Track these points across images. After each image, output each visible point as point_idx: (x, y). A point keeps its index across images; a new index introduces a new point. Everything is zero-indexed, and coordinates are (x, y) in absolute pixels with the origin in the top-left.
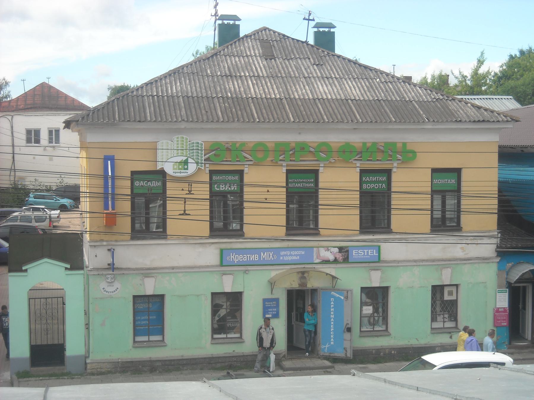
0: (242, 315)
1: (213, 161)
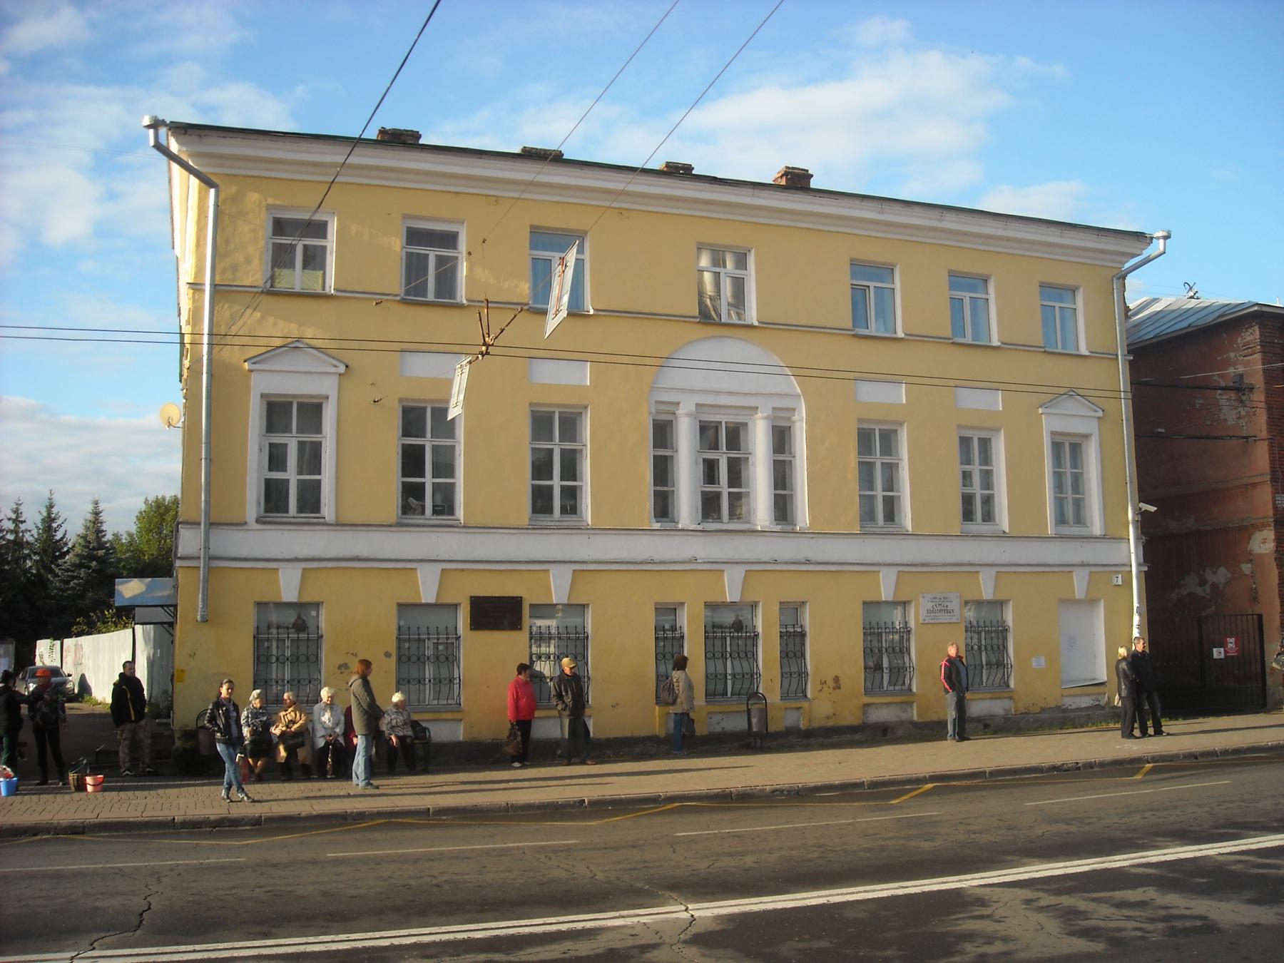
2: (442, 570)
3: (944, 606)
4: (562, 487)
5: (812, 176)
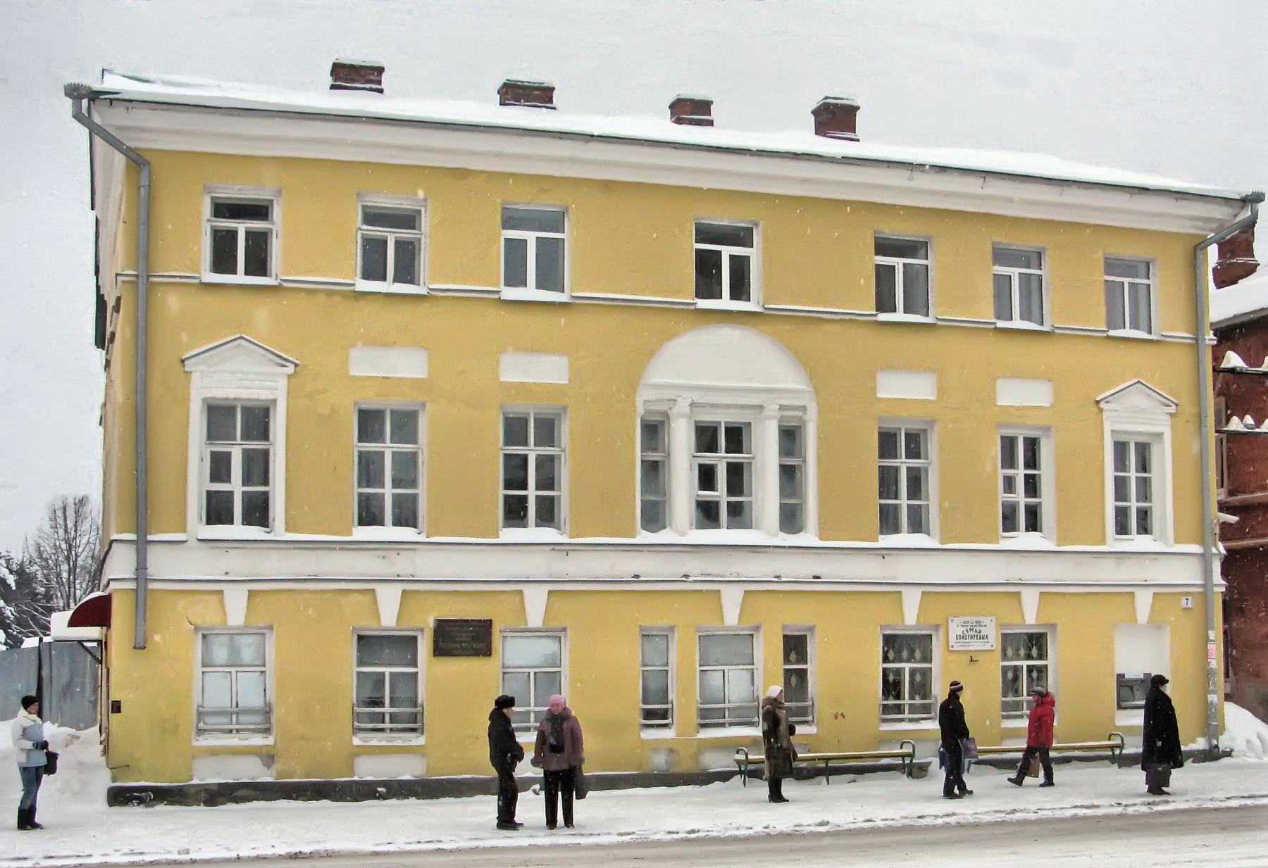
0: (412, 294)
1: (263, 686)
2: (403, 591)
3: (976, 631)
4: (537, 497)
5: (858, 108)
